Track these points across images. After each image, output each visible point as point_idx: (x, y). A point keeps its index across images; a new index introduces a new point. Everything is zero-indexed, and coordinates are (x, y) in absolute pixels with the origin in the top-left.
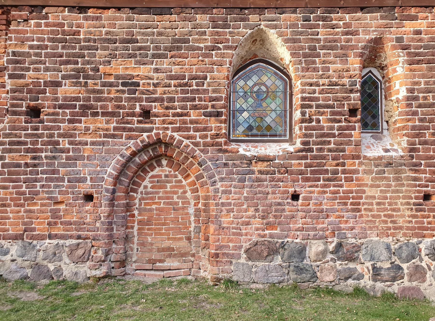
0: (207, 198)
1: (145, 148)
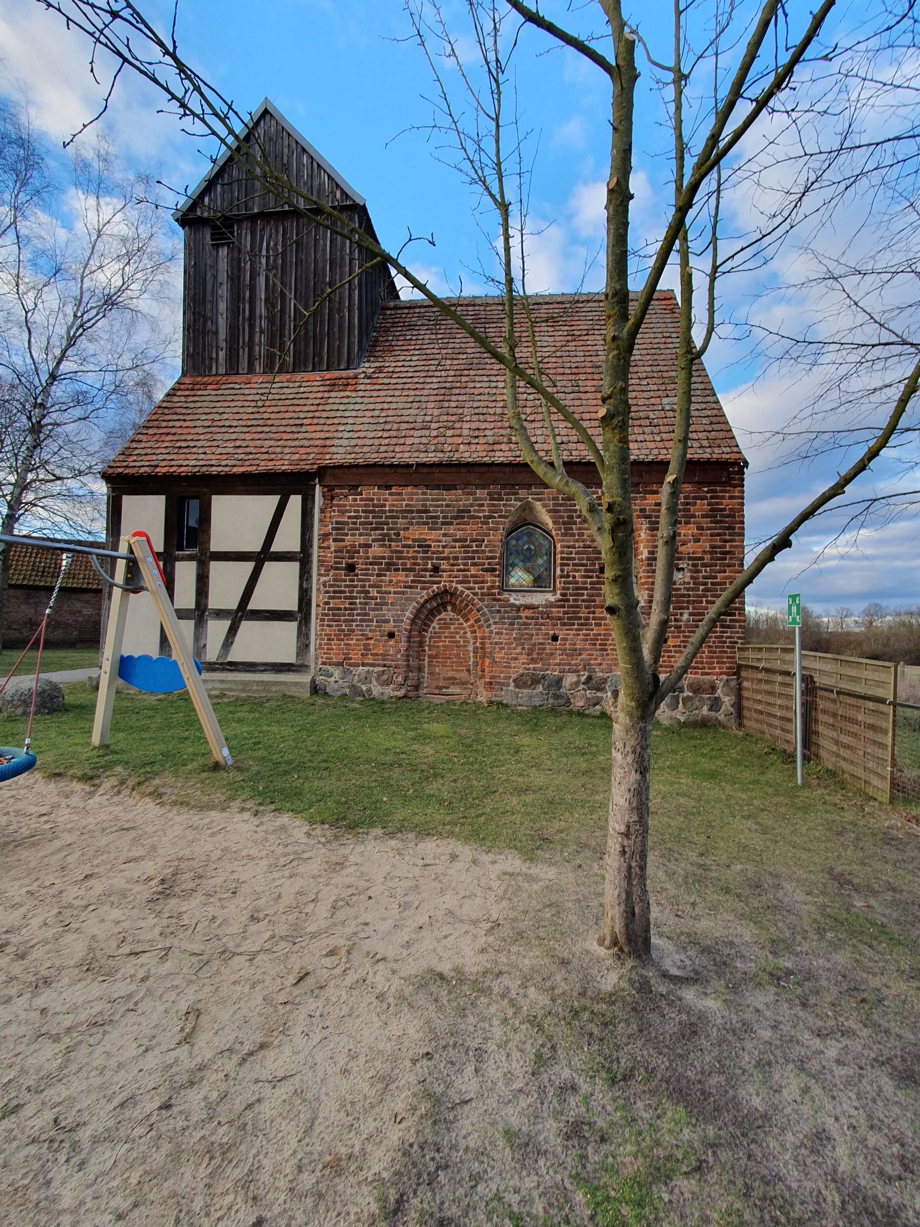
0: (483, 638)
1: (435, 596)
